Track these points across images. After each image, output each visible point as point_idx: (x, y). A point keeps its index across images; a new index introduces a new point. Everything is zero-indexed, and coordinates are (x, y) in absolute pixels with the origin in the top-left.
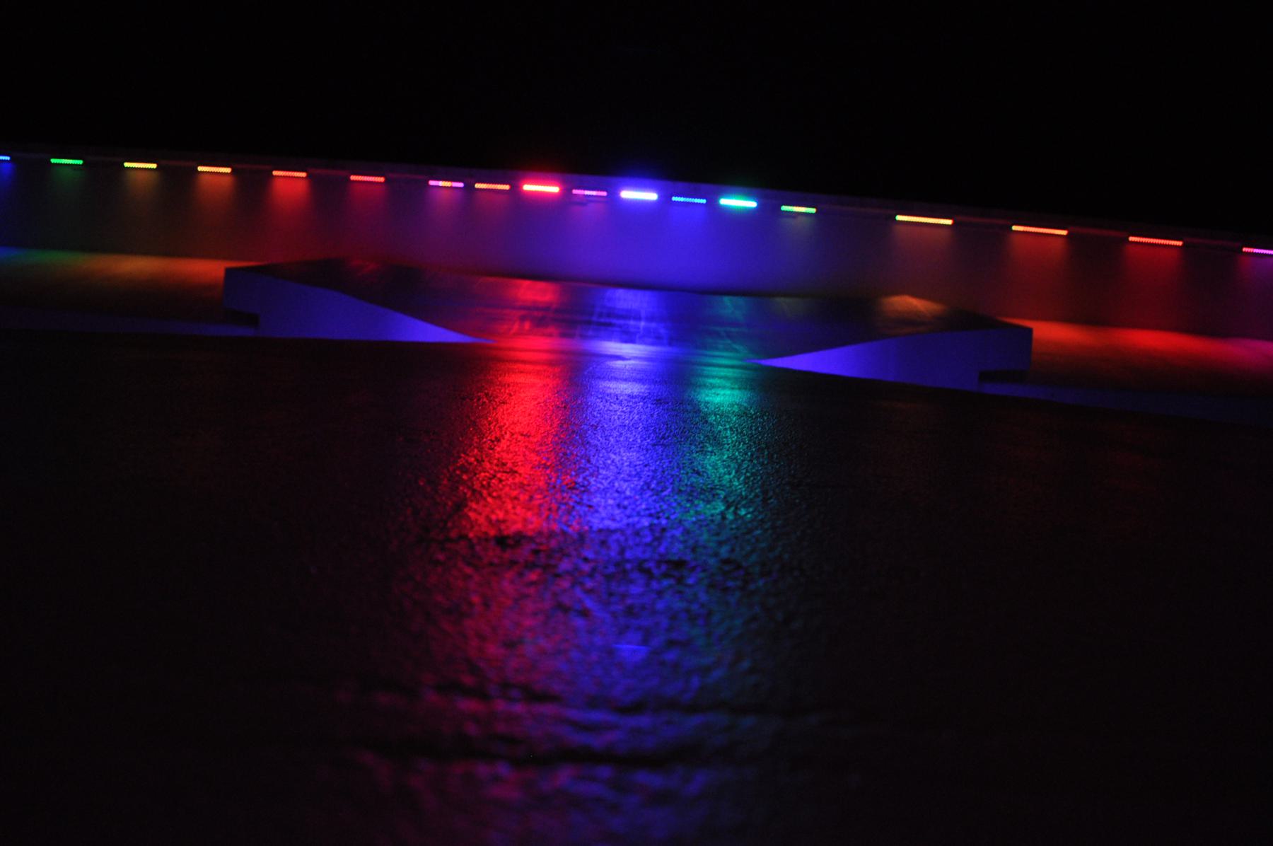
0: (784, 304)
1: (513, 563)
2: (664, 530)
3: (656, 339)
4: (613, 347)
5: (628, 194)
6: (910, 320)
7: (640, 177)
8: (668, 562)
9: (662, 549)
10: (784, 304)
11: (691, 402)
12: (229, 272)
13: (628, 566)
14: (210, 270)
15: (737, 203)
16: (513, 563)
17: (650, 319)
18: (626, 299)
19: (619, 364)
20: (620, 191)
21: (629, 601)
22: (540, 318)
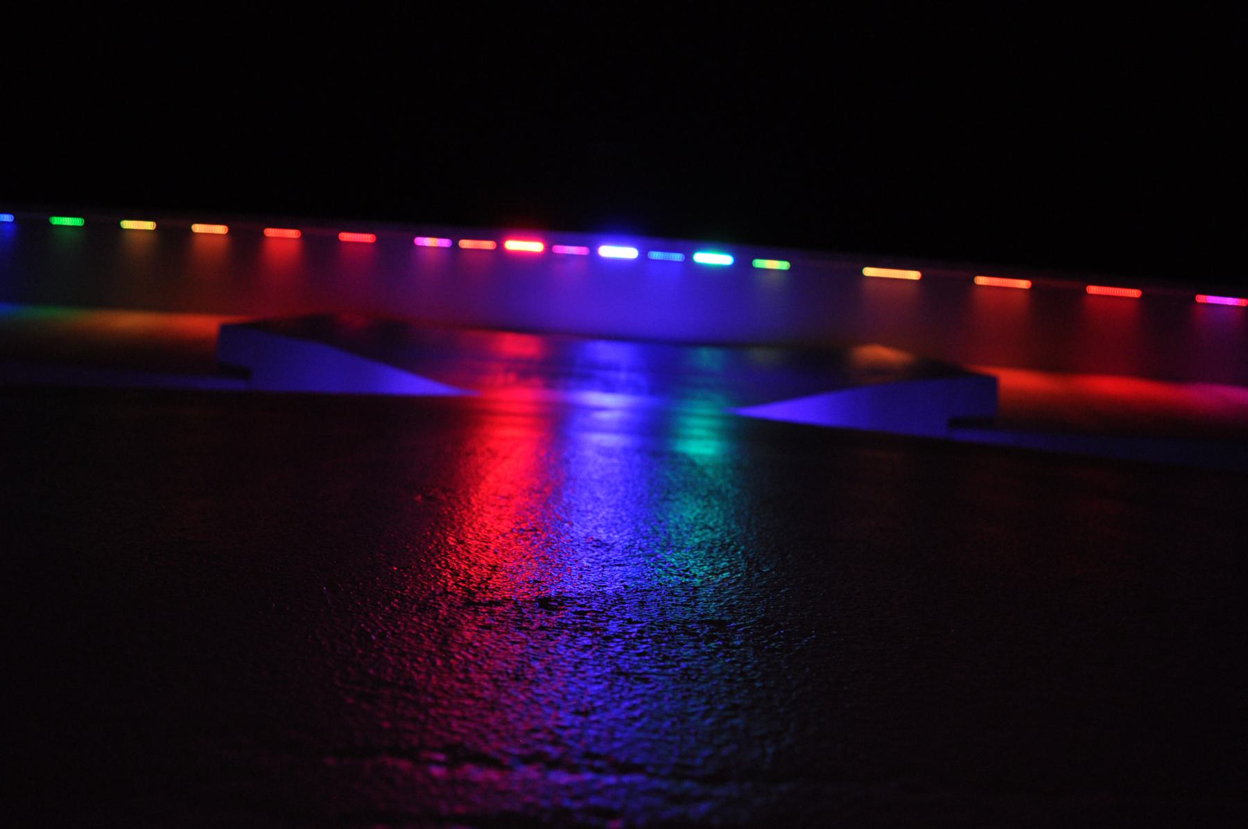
0: (760, 356)
1: (562, 626)
2: (695, 588)
3: (633, 388)
4: (595, 398)
5: (512, 245)
6: (880, 370)
7: (619, 235)
8: (710, 622)
9: (699, 610)
10: (760, 356)
11: (675, 455)
12: (224, 329)
13: (673, 628)
14: (203, 325)
15: (713, 258)
16: (562, 626)
17: (631, 370)
18: (607, 352)
19: (604, 416)
20: (598, 247)
21: (683, 665)
22: (525, 370)
